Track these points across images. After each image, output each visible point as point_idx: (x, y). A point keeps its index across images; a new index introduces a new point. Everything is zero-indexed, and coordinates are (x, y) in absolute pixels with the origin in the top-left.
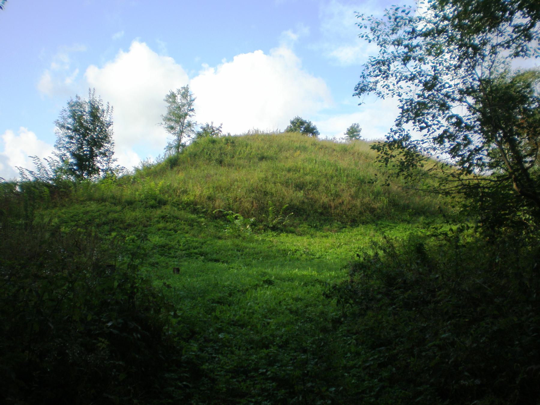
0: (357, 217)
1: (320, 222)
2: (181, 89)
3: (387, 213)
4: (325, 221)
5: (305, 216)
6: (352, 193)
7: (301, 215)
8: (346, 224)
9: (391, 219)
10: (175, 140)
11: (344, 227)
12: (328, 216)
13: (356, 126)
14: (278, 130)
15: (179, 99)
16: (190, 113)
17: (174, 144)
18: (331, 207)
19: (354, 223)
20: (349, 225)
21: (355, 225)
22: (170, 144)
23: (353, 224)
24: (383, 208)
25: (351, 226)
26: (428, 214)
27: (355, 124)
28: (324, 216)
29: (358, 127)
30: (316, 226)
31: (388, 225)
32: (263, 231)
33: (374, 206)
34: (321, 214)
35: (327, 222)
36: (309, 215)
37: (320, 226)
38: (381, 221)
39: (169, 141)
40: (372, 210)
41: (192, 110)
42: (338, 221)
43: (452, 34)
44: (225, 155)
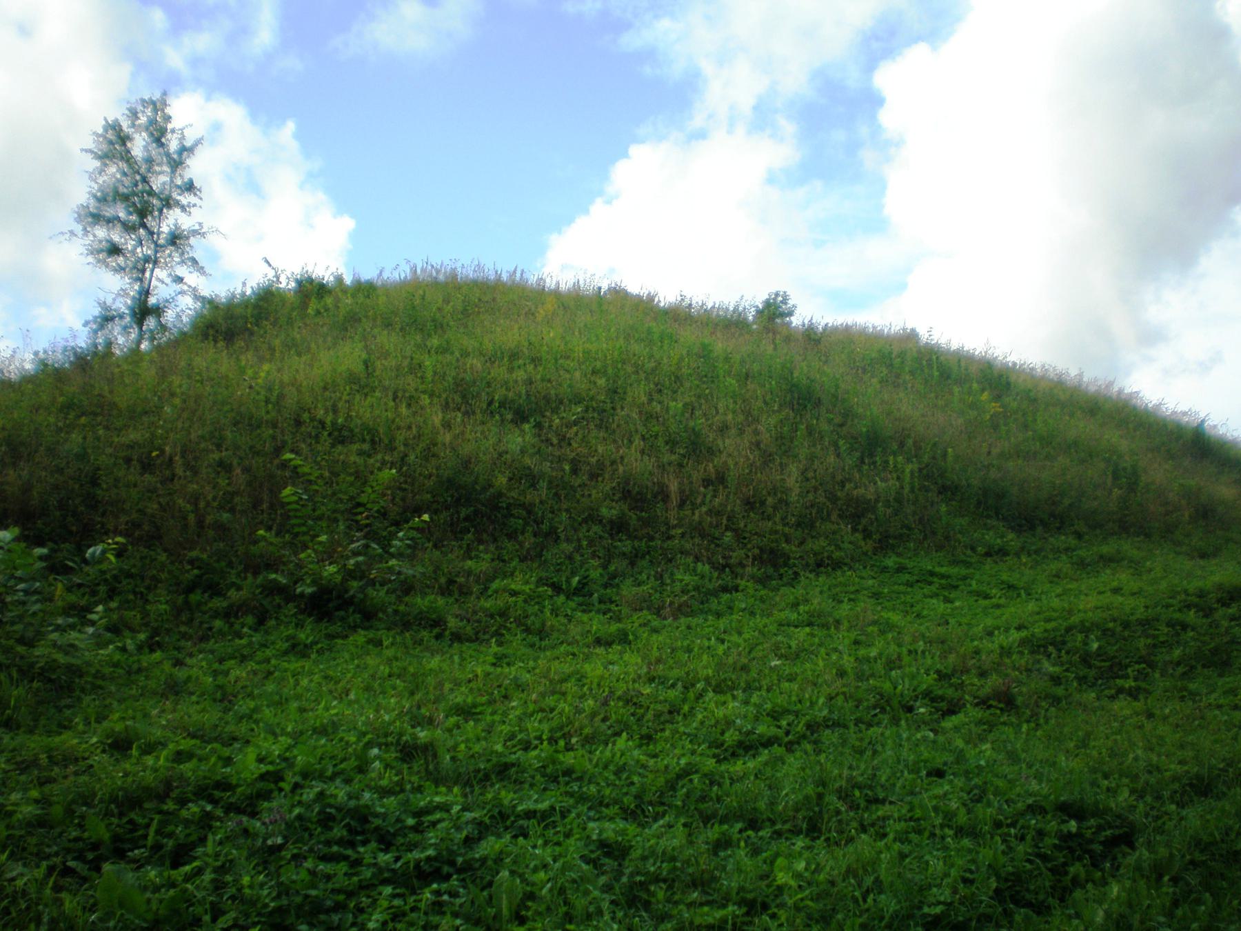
0: (788, 541)
1: (605, 567)
2: (140, 108)
3: (921, 520)
4: (632, 564)
5: (529, 541)
6: (766, 437)
7: (511, 536)
8: (735, 575)
9: (940, 548)
10: (123, 293)
11: (725, 589)
12: (652, 539)
13: (780, 299)
14: (518, 275)
15: (139, 146)
16: (185, 199)
17: (122, 305)
18: (666, 498)
19: (775, 566)
20: (753, 577)
21: (781, 577)
22: (104, 306)
23: (770, 571)
24: (899, 500)
25: (763, 581)
26: (1080, 526)
27: (777, 294)
28: (630, 537)
29: (785, 301)
30: (583, 584)
31: (932, 574)
32: (250, 620)
33: (862, 491)
34: (618, 527)
35: (644, 563)
36: (552, 535)
37: (605, 586)
38: (899, 555)
39: (102, 296)
40: (856, 512)
41: (190, 187)
42: (697, 559)
43: (587, 893)
44: (147, 260)
